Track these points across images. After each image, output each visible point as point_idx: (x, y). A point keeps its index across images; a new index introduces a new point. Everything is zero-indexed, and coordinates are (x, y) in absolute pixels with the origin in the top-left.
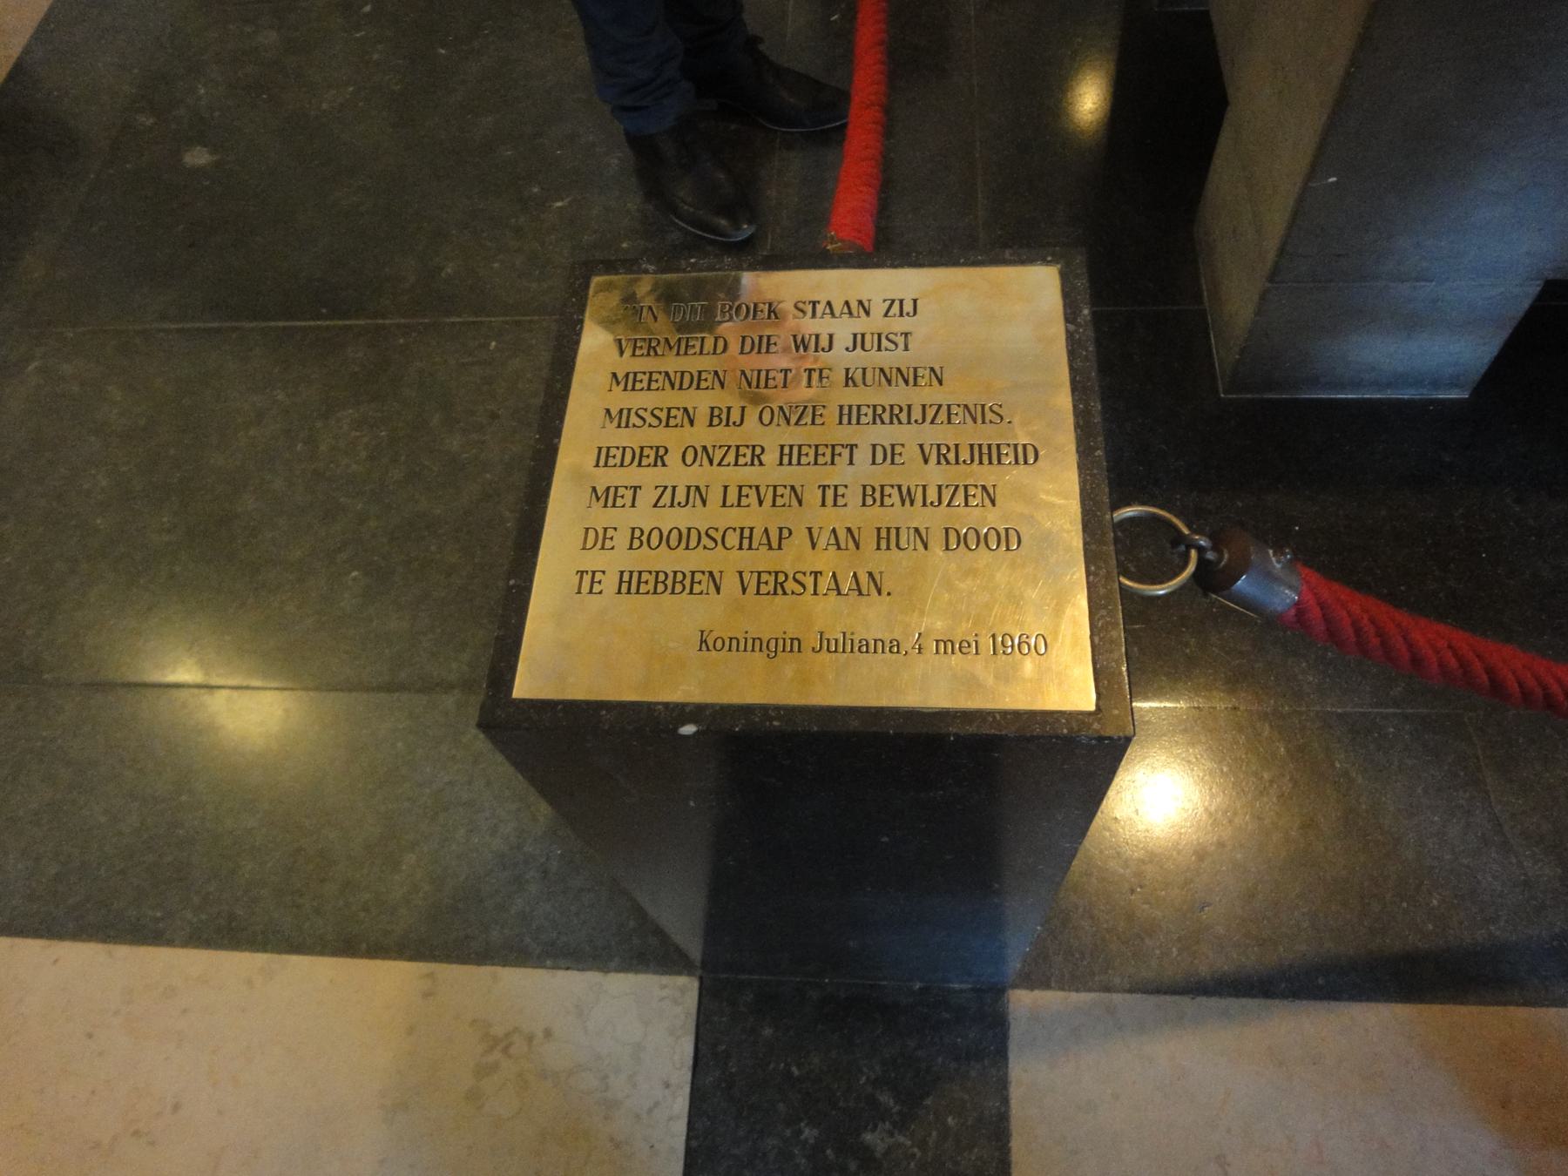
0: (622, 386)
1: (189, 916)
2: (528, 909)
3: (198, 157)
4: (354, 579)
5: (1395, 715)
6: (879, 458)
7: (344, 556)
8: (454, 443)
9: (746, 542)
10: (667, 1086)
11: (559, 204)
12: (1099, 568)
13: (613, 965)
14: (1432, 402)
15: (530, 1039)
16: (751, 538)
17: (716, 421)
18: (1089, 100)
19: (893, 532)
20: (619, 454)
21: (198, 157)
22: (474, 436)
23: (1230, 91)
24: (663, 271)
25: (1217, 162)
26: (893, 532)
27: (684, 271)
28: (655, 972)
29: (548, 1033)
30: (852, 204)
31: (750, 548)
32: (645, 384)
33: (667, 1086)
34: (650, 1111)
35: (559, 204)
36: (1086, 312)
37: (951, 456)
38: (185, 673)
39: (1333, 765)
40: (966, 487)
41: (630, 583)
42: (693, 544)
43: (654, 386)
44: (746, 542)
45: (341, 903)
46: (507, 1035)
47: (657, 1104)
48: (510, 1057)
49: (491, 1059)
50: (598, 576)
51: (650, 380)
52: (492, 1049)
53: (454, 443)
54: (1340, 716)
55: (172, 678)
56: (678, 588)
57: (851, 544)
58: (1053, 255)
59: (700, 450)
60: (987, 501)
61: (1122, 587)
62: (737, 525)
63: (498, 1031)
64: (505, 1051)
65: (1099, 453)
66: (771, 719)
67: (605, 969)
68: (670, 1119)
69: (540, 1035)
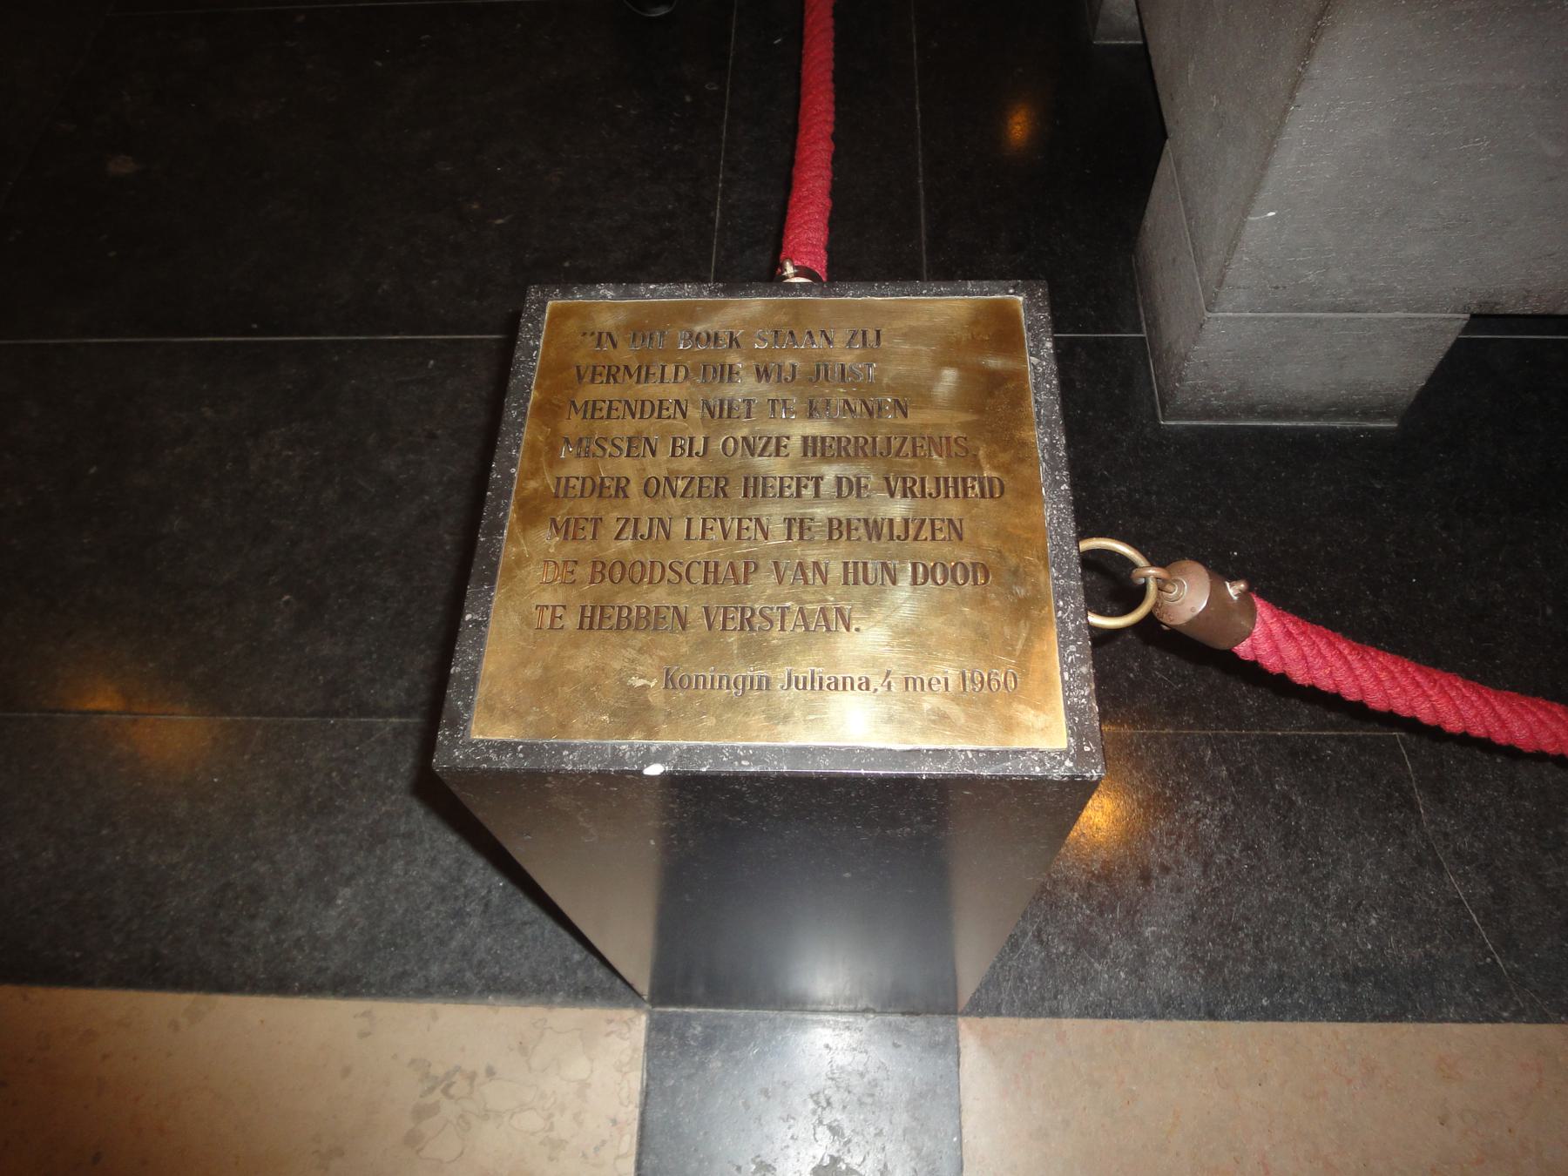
0: (581, 414)
1: (111, 956)
2: (468, 942)
3: (121, 166)
4: (287, 603)
5: (1332, 737)
6: (845, 490)
7: (274, 579)
8: (390, 463)
9: (711, 576)
10: (614, 1122)
11: (499, 221)
12: (1067, 603)
13: (558, 999)
14: (1362, 430)
15: (472, 1077)
16: (716, 571)
17: (679, 451)
18: (1019, 127)
19: (860, 566)
20: (579, 484)
21: (121, 166)
22: (411, 456)
23: (1169, 125)
24: (621, 298)
25: (1157, 191)
26: (860, 566)
27: (643, 297)
28: (603, 1006)
29: (491, 1072)
30: (809, 233)
31: (716, 582)
32: (605, 413)
33: (614, 1122)
34: (597, 1149)
35: (499, 221)
36: (1049, 345)
37: (917, 489)
38: (104, 699)
39: (1272, 786)
40: (933, 522)
41: (592, 617)
42: (657, 576)
43: (614, 414)
44: (711, 576)
45: (272, 938)
46: (448, 1075)
47: (604, 1142)
48: (451, 1097)
49: (431, 1099)
50: (559, 611)
51: (610, 408)
52: (431, 1089)
53: (390, 463)
54: (1278, 739)
55: (91, 706)
56: (643, 624)
57: (819, 581)
58: (1014, 287)
59: (663, 481)
60: (954, 536)
61: (1092, 628)
62: (606, 501)
63: (438, 1070)
64: (445, 1092)
65: (1065, 487)
66: (739, 759)
67: (549, 1003)
68: (618, 1157)
69: (482, 1072)
